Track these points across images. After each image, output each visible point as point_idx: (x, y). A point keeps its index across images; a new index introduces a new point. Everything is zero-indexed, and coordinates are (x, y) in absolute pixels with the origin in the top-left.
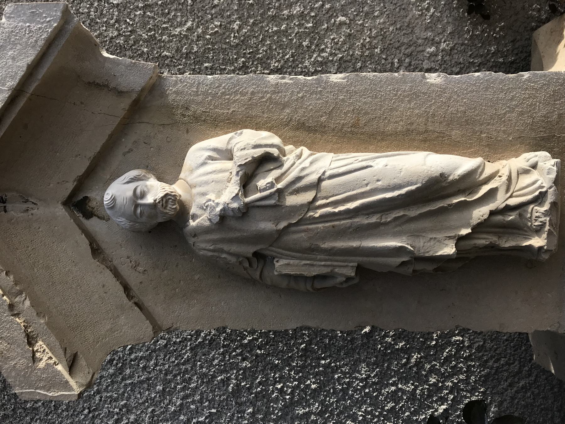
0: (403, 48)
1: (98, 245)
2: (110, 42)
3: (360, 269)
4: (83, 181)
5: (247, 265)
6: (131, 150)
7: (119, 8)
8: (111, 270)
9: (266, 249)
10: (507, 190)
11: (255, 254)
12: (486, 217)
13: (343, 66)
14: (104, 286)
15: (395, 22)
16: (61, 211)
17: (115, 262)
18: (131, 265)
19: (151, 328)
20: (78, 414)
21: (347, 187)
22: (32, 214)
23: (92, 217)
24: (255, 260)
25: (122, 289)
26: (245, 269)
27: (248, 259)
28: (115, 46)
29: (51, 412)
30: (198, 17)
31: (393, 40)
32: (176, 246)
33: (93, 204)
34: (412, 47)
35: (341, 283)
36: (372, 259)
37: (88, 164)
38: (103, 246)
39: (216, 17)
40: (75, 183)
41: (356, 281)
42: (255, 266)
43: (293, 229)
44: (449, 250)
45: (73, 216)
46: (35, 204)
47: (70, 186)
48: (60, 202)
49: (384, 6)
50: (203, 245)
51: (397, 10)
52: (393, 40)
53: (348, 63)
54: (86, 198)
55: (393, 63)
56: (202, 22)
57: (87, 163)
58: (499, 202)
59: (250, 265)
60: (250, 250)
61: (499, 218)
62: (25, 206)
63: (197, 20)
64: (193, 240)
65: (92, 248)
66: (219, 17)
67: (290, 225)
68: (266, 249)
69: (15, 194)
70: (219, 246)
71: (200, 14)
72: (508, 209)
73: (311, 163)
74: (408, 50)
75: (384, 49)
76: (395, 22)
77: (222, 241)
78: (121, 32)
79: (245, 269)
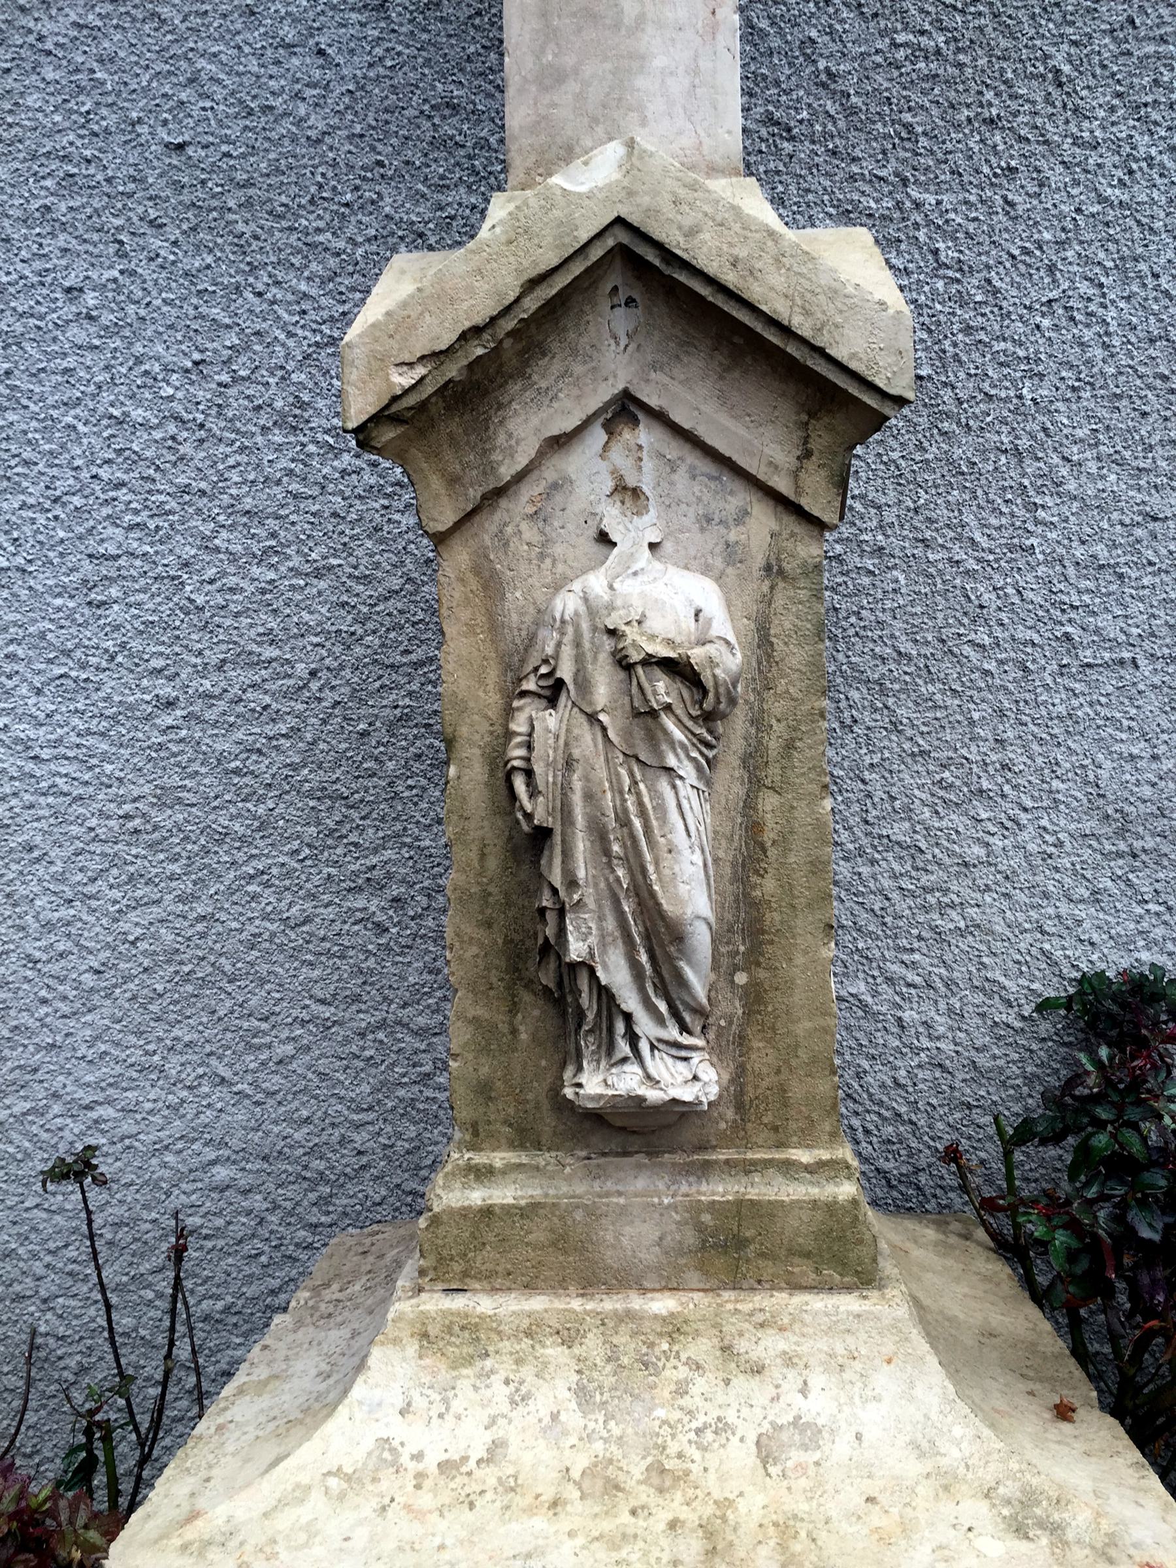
0: (943, 971)
1: (565, 444)
2: (945, 384)
3: (542, 835)
5: (544, 670)
7: (1015, 401)
9: (569, 696)
10: (660, 1040)
11: (560, 684)
12: (623, 1006)
13: (904, 853)
15: (995, 954)
20: (191, 339)
21: (661, 809)
24: (550, 682)
26: (536, 669)
28: (937, 395)
29: (192, 283)
30: (997, 560)
31: (957, 951)
35: (522, 808)
36: (558, 850)
39: (999, 597)
41: (525, 827)
42: (542, 683)
44: (576, 949)
45: (607, 405)
47: (653, 402)
49: (1026, 931)
51: (1018, 957)
52: (957, 951)
53: (909, 863)
56: (989, 569)
59: (543, 676)
60: (566, 672)
61: (620, 1027)
63: (991, 557)
66: (999, 602)
67: (604, 729)
68: (569, 696)
70: (570, 630)
71: (1003, 563)
72: (633, 1039)
74: (937, 979)
76: (995, 954)
78: (965, 405)
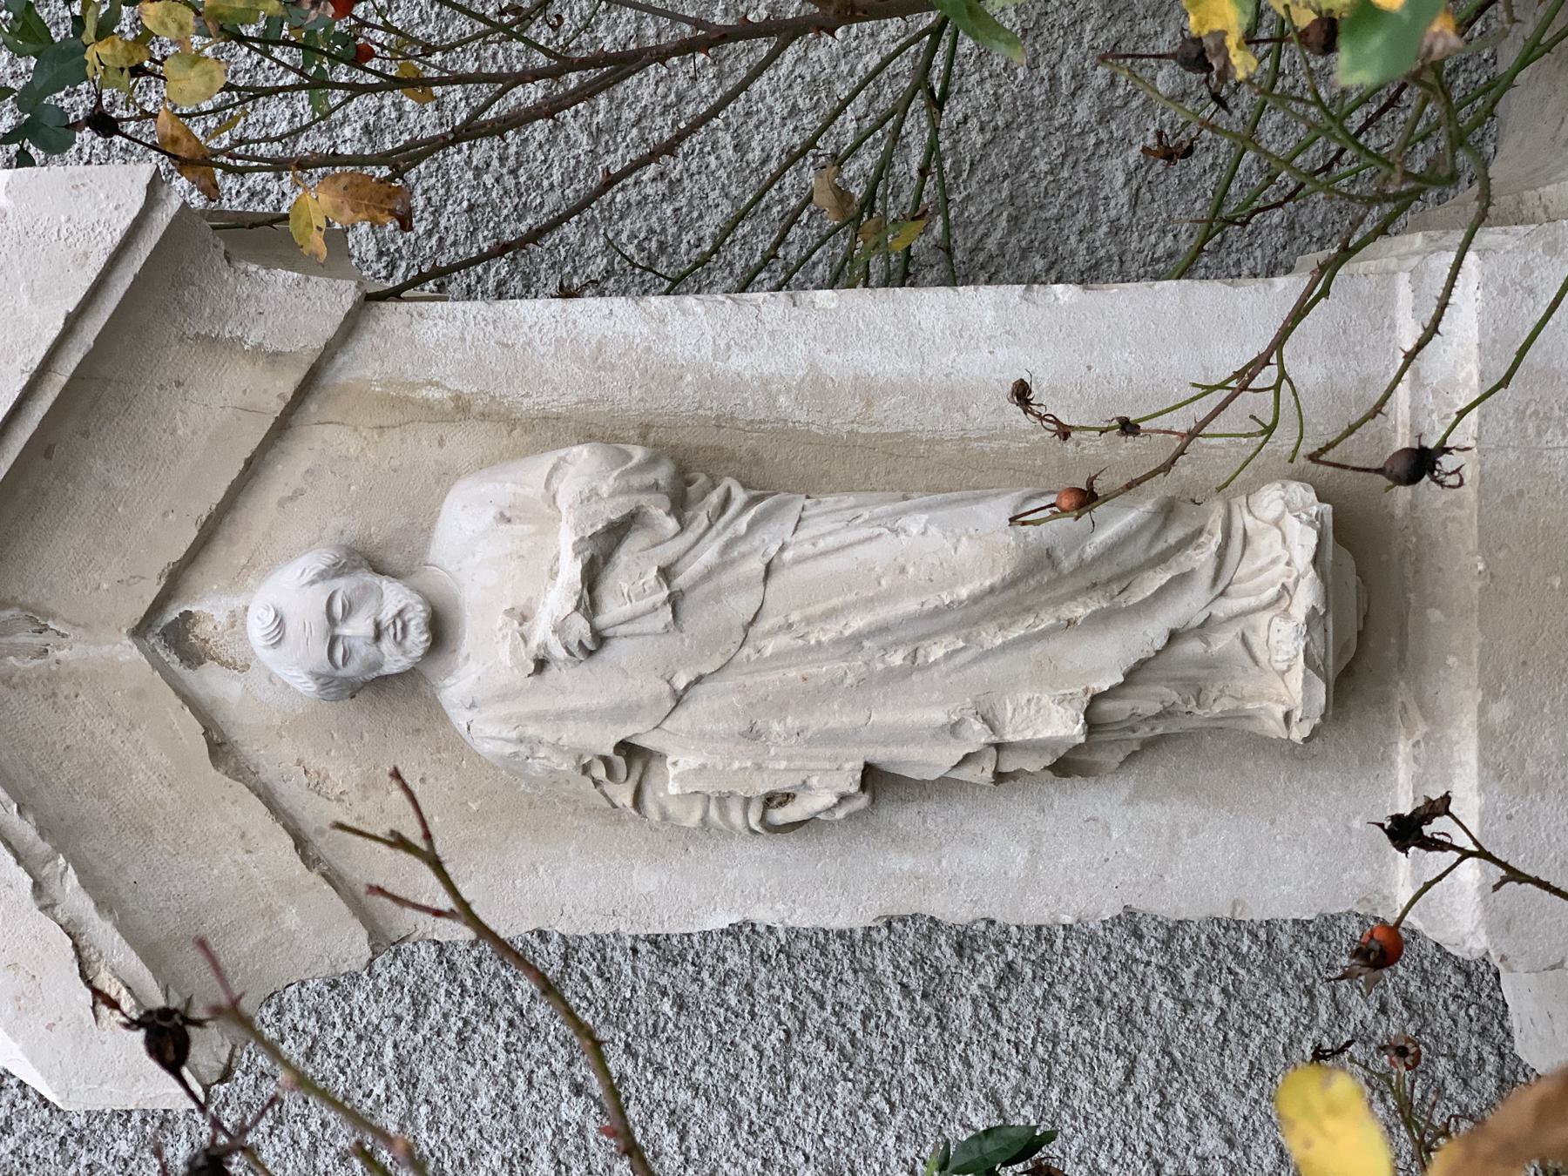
4: (175, 581)
5: (600, 772)
6: (298, 493)
8: (259, 796)
10: (1215, 580)
14: (243, 836)
16: (127, 652)
17: (263, 777)
18: (305, 780)
19: (363, 935)
22: (58, 662)
23: (201, 663)
24: (620, 761)
25: (291, 842)
26: (597, 783)
27: (606, 760)
32: (418, 730)
33: (202, 630)
34: (1120, 24)
37: (196, 533)
38: (236, 736)
40: (163, 581)
43: (743, 548)
46: (63, 636)
47: (151, 590)
48: (124, 630)
50: (490, 730)
54: (187, 615)
55: (1054, 79)
57: (192, 533)
58: (1189, 607)
59: (611, 773)
62: (38, 640)
64: (469, 715)
65: (209, 742)
69: (15, 612)
73: (752, 526)
74: (1104, 36)
75: (1025, 31)
77: (538, 717)
79: (597, 783)
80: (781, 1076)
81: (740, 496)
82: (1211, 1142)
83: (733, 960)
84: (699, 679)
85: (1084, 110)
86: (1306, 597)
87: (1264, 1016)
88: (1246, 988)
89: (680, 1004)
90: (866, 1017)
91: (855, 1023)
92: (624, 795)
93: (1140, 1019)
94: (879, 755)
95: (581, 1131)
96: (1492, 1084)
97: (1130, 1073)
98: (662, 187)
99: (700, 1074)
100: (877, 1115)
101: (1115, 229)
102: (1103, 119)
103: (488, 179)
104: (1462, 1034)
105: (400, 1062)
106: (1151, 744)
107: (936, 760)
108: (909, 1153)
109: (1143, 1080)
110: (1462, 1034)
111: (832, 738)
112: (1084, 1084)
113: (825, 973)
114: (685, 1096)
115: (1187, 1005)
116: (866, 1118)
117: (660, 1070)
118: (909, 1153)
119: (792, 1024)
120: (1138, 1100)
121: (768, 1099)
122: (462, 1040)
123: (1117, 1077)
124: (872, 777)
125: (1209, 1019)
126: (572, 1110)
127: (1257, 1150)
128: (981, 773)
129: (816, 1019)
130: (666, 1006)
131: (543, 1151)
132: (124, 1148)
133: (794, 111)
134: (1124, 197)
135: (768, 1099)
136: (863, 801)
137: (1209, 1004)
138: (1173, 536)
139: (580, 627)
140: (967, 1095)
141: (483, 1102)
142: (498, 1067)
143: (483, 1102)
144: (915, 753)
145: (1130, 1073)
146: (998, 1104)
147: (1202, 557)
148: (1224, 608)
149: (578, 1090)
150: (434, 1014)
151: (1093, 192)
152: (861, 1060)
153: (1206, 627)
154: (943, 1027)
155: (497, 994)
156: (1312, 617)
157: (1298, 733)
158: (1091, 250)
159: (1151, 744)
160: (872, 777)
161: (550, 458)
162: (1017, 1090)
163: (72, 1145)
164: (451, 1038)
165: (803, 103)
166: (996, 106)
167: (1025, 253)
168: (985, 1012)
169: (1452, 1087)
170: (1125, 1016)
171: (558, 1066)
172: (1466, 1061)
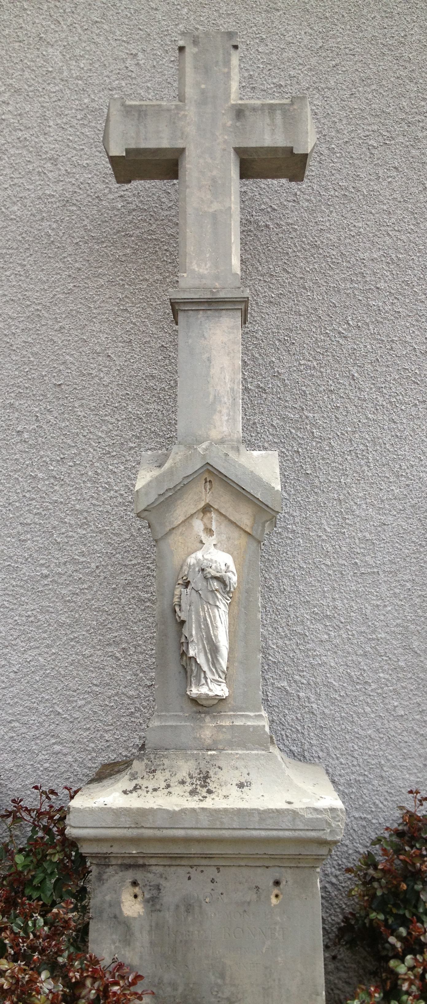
44: (192, 653)
58: (209, 675)
80: (98, 610)
81: (228, 602)
82: (80, 703)
83: (123, 600)
84: (200, 595)
85: (297, 677)
86: (211, 694)
87: (107, 715)
88: (113, 711)
89: (114, 589)
90: (110, 628)
91: (109, 626)
92: (180, 582)
93: (107, 687)
94: (187, 623)
95: (88, 568)
96: (90, 765)
97: (96, 685)
98: (282, 590)
99: (99, 593)
100: (89, 630)
101: (273, 684)
102: (295, 681)
103: (285, 554)
104: (101, 759)
105: (105, 530)
106: (185, 669)
107: (185, 632)
108: (80, 637)
109: (95, 688)
110: (101, 759)
111: (190, 616)
112: (93, 675)
113: (120, 619)
114: (95, 589)
115: (109, 698)
116: (88, 628)
117: (100, 584)
118: (80, 637)
119: (109, 613)
120: (90, 687)
121: (93, 607)
122: (109, 543)
123: (95, 682)
124: (183, 622)
125: (107, 703)
126: (93, 565)
127: (78, 713)
128: (183, 640)
129: (110, 617)
130: (114, 586)
131: (85, 559)
132: (90, 473)
133: (297, 617)
134: (279, 686)
135: (93, 607)
136: (179, 621)
137: (110, 702)
138: (221, 674)
139: (209, 576)
140: (92, 650)
141: (96, 547)
142: (103, 551)
143: (96, 547)
144: (187, 629)
145: (96, 685)
146: (90, 656)
147: (217, 677)
148: (209, 681)
149: (97, 567)
150: (115, 538)
151: (280, 679)
152: (101, 627)
153: (206, 678)
154: (107, 645)
155: (118, 551)
156: (207, 695)
157: (188, 693)
158: (269, 679)
159: (185, 669)
160: (183, 622)
161: (235, 572)
162: (93, 660)
163: (91, 463)
164: (110, 541)
165: (299, 619)
166: (298, 659)
167: (268, 665)
168: (110, 654)
169: (89, 757)
170: (108, 684)
171: (103, 563)
172: (95, 760)
